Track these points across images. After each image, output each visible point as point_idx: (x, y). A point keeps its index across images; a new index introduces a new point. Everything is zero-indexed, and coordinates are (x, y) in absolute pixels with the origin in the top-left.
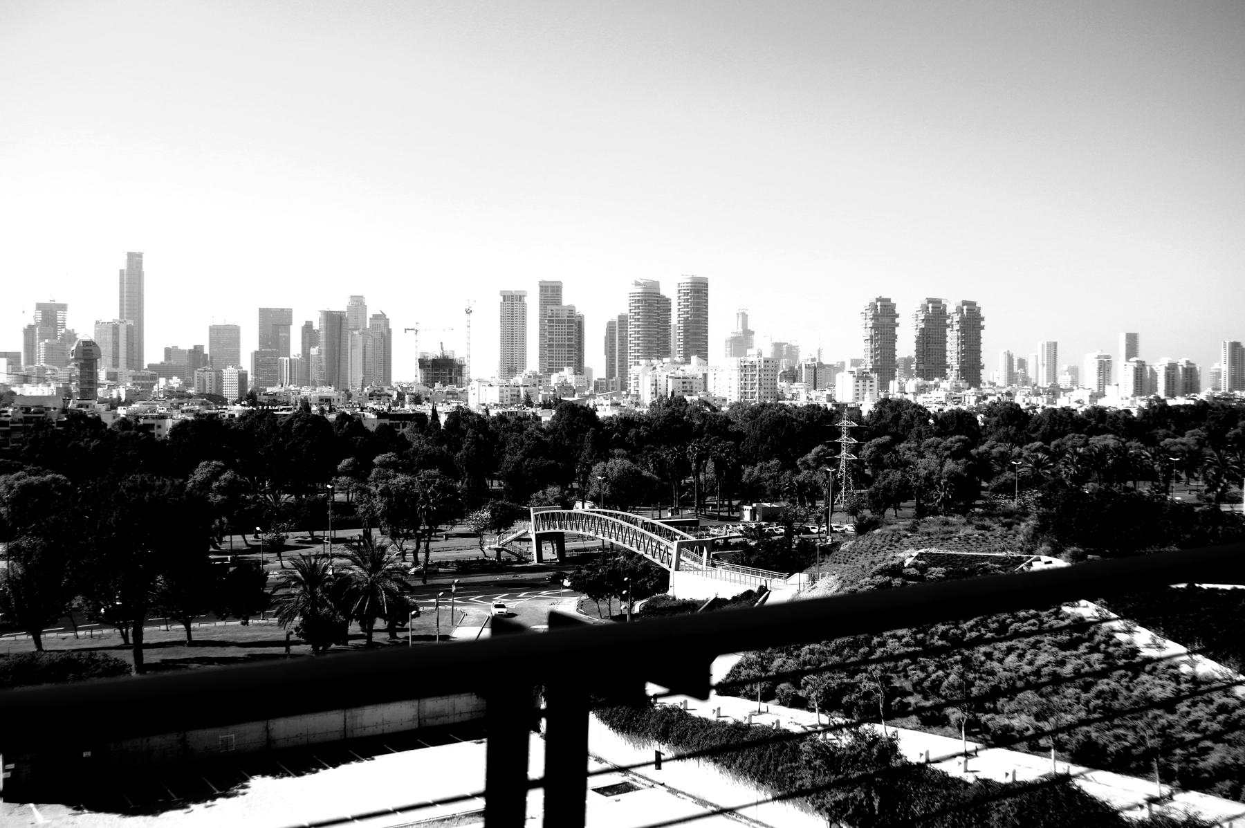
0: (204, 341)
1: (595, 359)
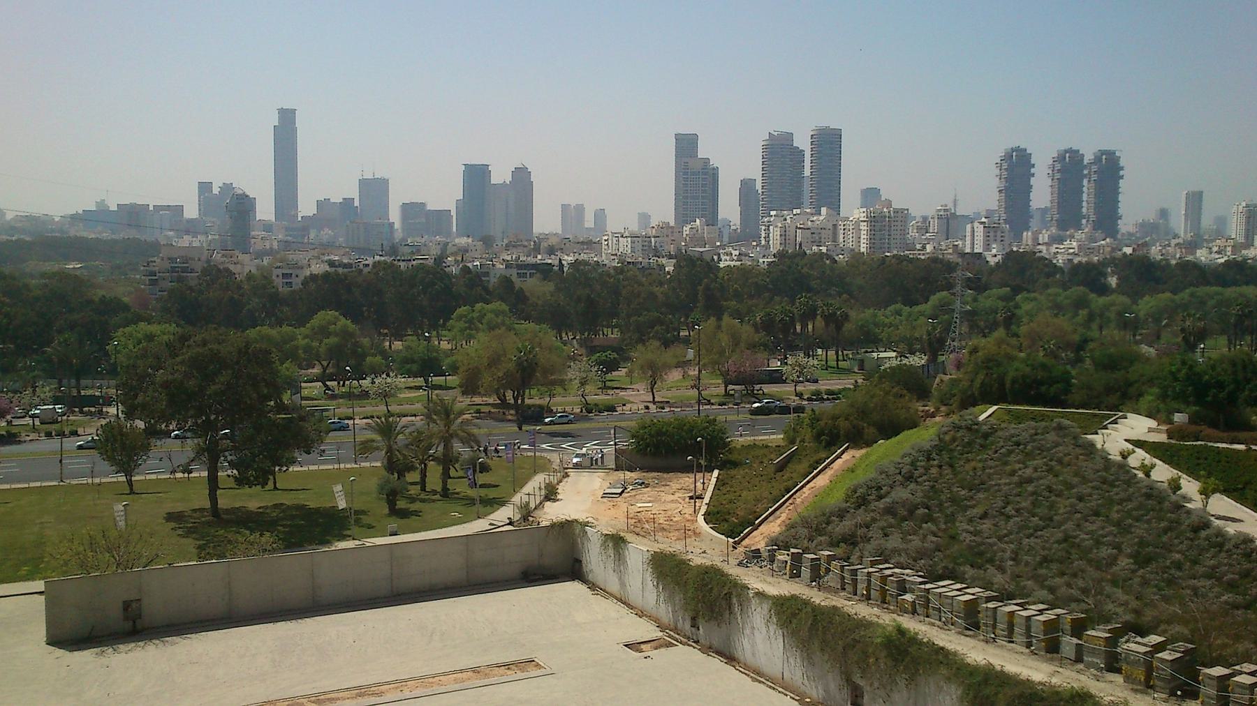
0: (354, 194)
1: (729, 209)
